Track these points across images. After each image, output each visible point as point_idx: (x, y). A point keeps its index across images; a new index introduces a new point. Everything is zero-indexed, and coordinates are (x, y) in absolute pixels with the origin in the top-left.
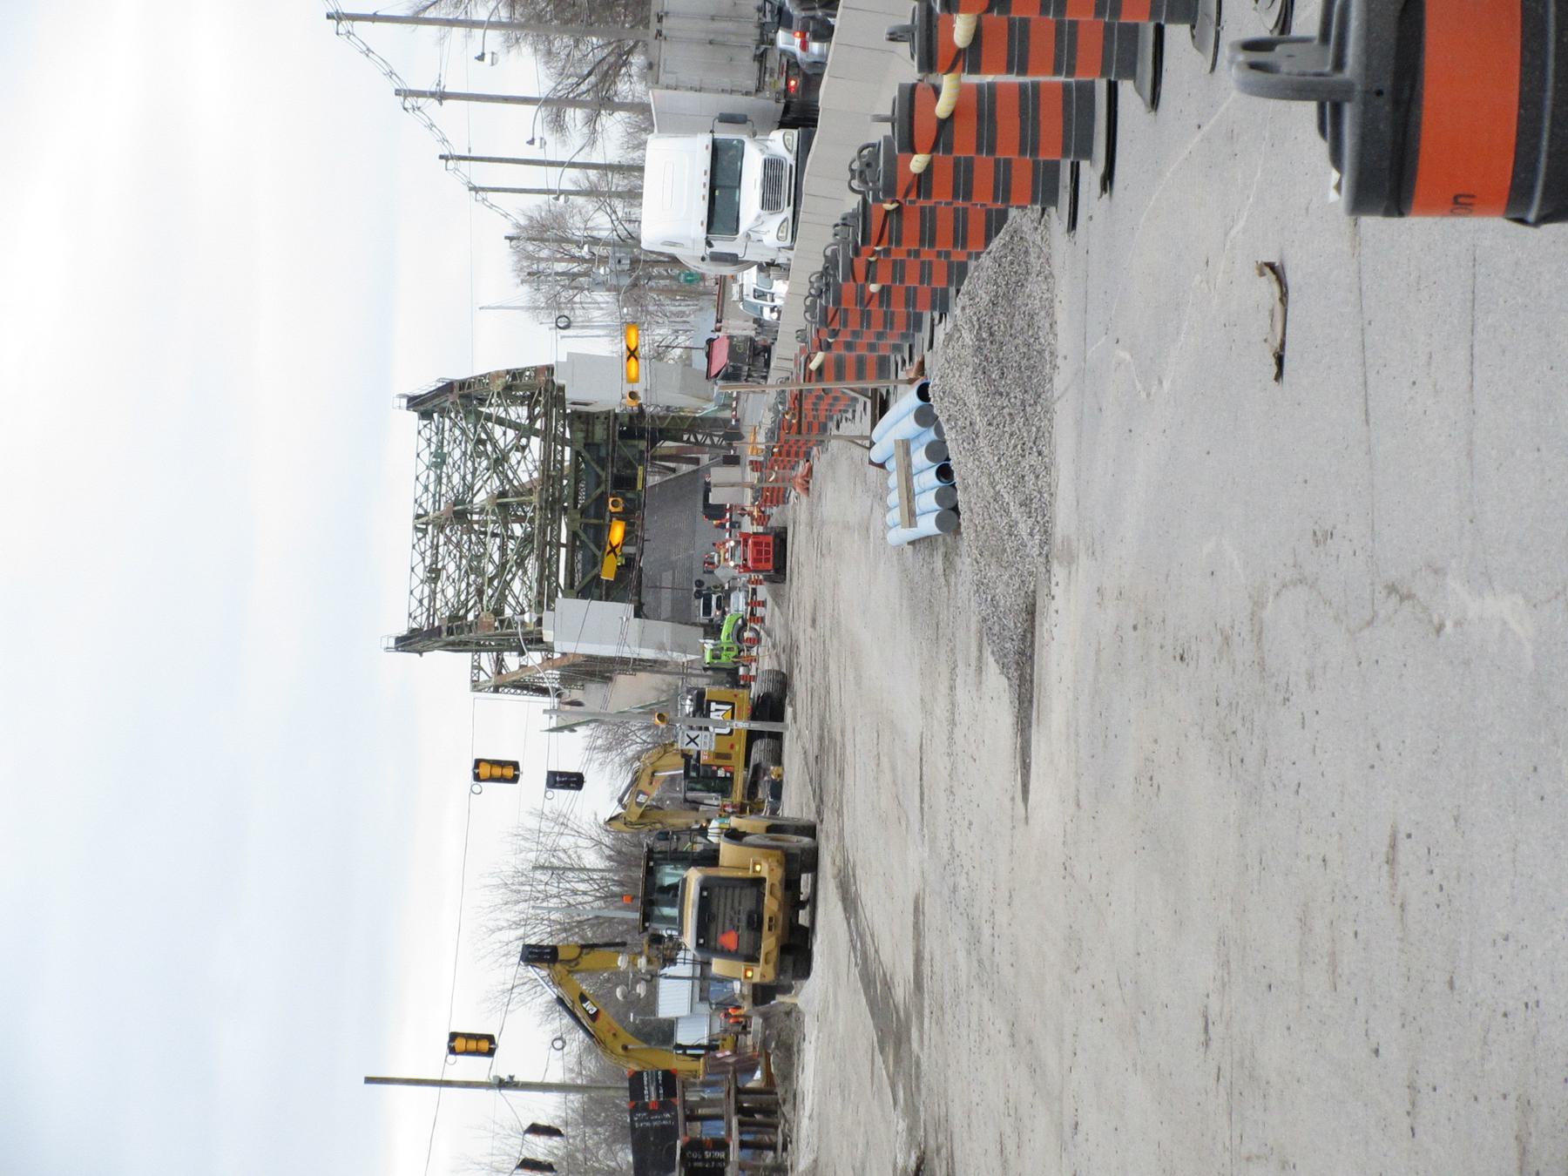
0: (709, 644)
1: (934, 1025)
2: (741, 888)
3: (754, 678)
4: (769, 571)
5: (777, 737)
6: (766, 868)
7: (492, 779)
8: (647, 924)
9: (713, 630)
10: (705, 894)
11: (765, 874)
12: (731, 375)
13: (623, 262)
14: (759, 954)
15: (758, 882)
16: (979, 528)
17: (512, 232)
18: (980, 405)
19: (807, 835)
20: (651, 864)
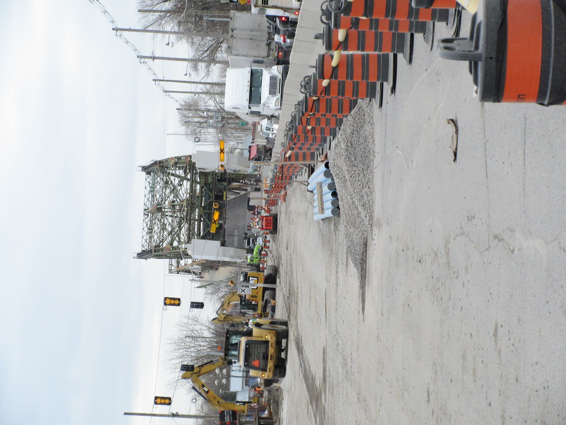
0: (249, 256)
1: (330, 394)
2: (261, 345)
3: (266, 268)
4: (271, 230)
5: (274, 290)
6: (270, 337)
7: (170, 304)
8: (226, 357)
9: (250, 251)
10: (247, 346)
11: (269, 339)
12: (258, 159)
13: (219, 118)
14: (267, 368)
15: (267, 342)
16: (347, 214)
17: (179, 107)
18: (347, 170)
19: (284, 325)
20: (228, 335)
